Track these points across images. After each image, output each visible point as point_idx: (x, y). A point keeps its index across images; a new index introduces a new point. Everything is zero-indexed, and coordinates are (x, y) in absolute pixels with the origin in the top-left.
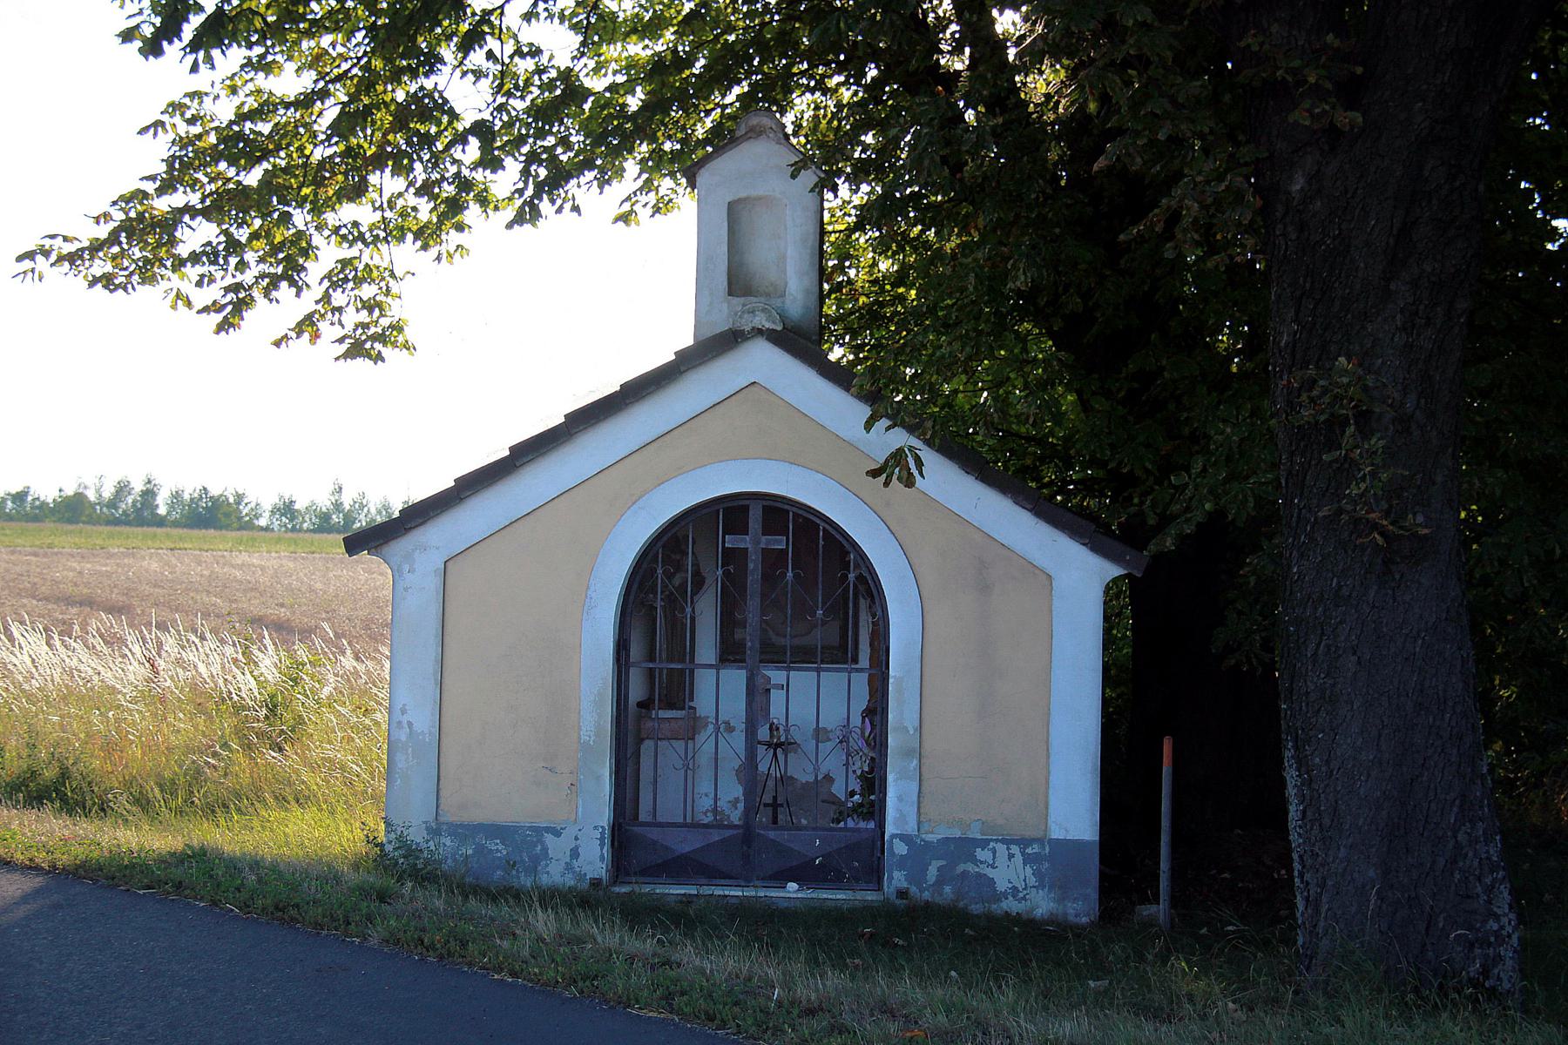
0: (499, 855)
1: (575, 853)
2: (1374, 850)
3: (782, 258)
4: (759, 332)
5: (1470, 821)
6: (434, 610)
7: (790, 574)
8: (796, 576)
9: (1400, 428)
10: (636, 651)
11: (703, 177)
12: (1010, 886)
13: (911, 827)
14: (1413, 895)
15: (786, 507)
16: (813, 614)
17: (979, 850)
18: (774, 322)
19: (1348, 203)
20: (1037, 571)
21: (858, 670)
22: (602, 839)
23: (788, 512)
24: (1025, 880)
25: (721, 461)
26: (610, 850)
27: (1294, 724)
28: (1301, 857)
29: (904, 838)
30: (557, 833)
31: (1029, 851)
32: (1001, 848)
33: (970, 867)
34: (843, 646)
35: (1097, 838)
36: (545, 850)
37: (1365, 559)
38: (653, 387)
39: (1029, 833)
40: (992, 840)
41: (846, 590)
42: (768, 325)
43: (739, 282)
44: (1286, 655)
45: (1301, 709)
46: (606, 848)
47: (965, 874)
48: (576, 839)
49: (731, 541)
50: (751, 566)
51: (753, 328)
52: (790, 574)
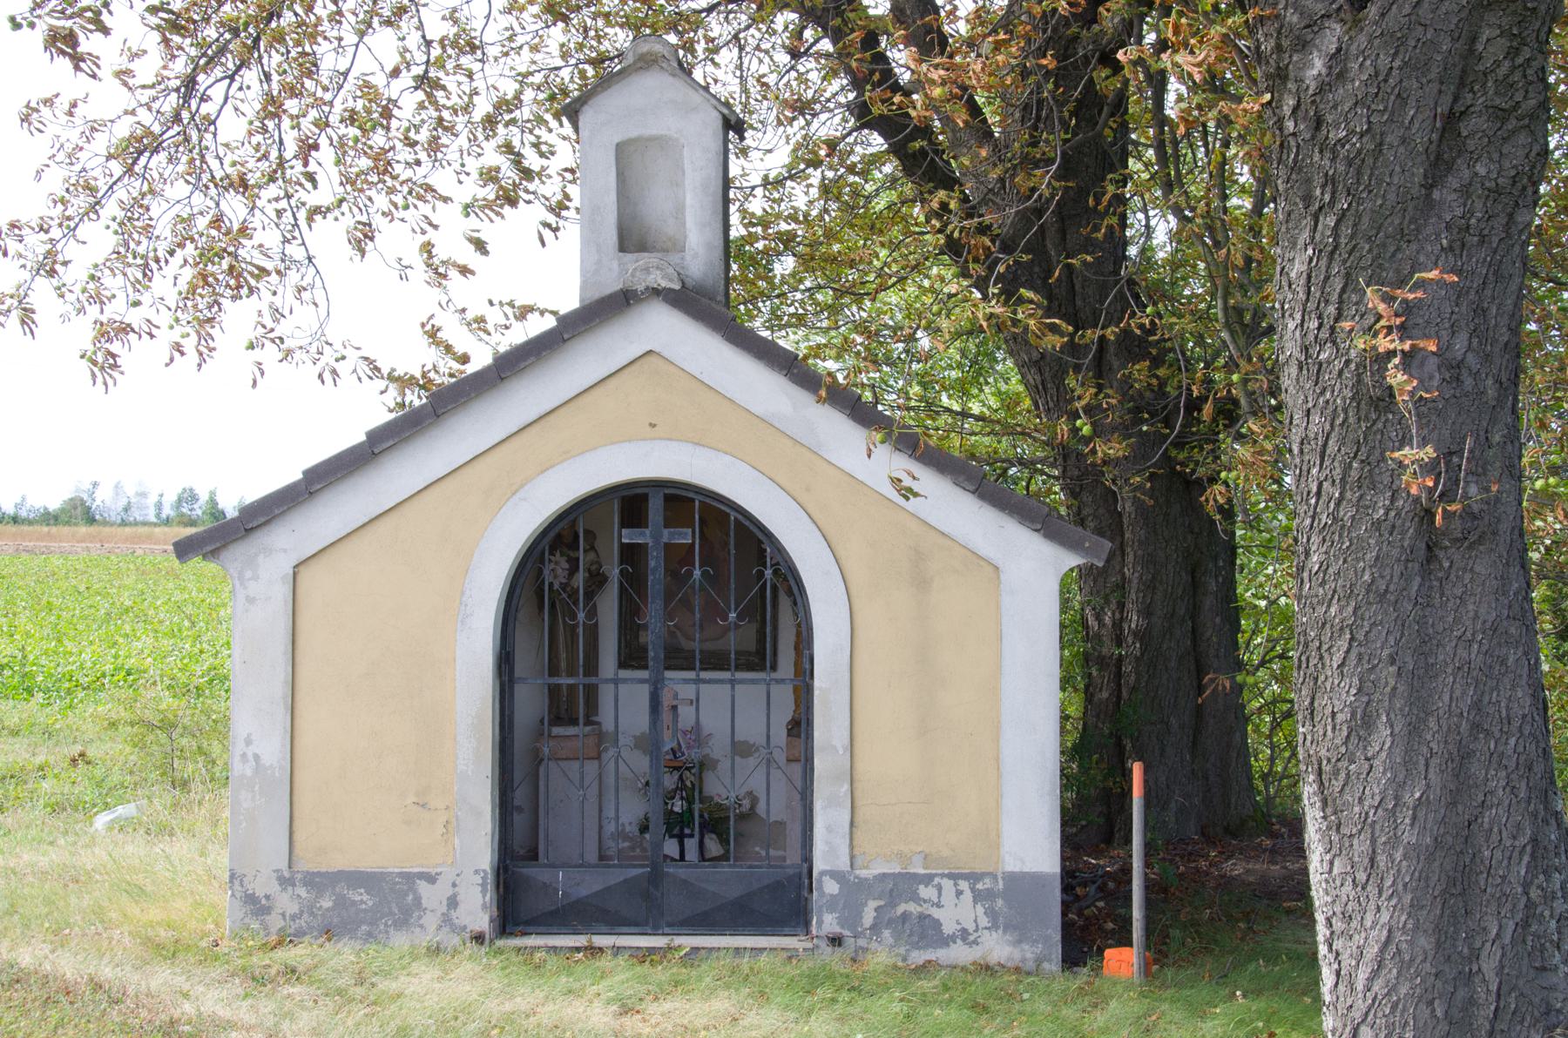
0: (364, 906)
1: (453, 902)
2: (1425, 912)
3: (680, 210)
4: (656, 292)
5: (1544, 873)
6: (283, 624)
7: (697, 573)
8: (704, 574)
9: (1447, 376)
10: (524, 663)
11: (587, 117)
12: (959, 927)
13: (843, 863)
14: (1475, 968)
15: (691, 495)
16: (725, 618)
17: (921, 887)
18: (671, 280)
19: (1379, 88)
20: (982, 563)
21: (778, 681)
22: (483, 885)
23: (693, 500)
24: (975, 921)
25: (612, 443)
26: (495, 897)
27: (1317, 753)
28: (1328, 920)
29: (835, 875)
30: (431, 879)
31: (979, 886)
32: (947, 884)
33: (912, 908)
34: (761, 652)
35: (1058, 870)
36: (418, 899)
37: (1406, 544)
38: (533, 359)
39: (979, 868)
40: (936, 875)
41: (764, 587)
42: (664, 284)
43: (632, 238)
44: (1304, 666)
45: (1325, 735)
46: (488, 895)
47: (905, 916)
48: (454, 885)
49: (629, 536)
50: (652, 563)
51: (647, 288)
52: (697, 573)
